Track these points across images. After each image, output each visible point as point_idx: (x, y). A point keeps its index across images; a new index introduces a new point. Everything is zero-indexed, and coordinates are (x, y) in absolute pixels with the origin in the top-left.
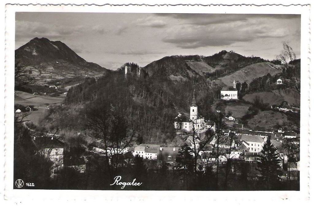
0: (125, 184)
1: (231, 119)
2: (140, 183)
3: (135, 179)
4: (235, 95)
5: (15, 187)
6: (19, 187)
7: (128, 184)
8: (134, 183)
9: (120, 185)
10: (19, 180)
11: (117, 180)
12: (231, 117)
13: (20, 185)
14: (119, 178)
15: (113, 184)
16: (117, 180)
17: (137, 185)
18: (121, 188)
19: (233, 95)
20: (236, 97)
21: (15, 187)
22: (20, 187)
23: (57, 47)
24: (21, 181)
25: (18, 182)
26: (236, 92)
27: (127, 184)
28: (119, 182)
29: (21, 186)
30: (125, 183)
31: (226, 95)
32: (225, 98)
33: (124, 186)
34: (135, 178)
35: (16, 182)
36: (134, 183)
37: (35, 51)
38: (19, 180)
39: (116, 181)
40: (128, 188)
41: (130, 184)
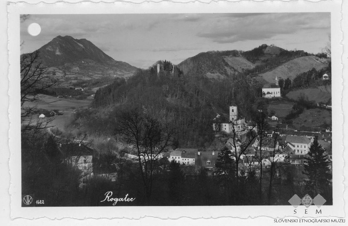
0: (117, 200)
2: (133, 199)
3: (127, 195)
4: (278, 93)
7: (120, 200)
8: (126, 199)
9: (111, 201)
11: (108, 196)
13: (28, 202)
14: (110, 193)
16: (108, 196)
19: (275, 93)
21: (24, 205)
22: (29, 204)
24: (30, 197)
25: (26, 198)
26: (278, 90)
27: (119, 200)
28: (110, 198)
29: (30, 203)
30: (117, 199)
32: (267, 96)
33: (116, 202)
38: (27, 196)
39: (107, 196)
40: (120, 204)
41: (122, 199)
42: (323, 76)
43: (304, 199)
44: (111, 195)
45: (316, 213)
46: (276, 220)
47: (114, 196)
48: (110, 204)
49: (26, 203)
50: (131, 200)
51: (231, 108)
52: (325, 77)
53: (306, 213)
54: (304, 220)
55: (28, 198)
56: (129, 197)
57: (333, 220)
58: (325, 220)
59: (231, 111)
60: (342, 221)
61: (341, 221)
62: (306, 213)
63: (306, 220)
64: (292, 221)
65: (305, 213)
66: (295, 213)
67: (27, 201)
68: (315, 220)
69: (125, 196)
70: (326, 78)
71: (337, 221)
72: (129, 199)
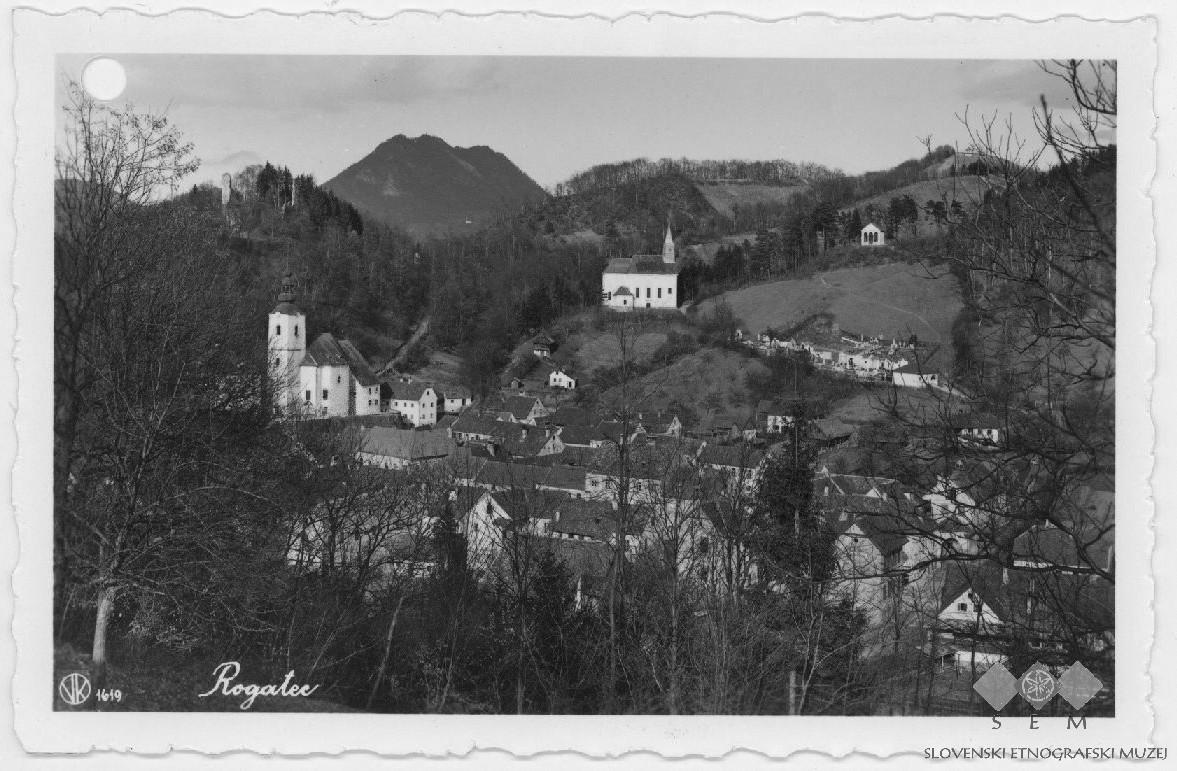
0: (254, 691)
1: (557, 383)
2: (311, 688)
3: (291, 674)
4: (665, 292)
5: (60, 704)
6: (74, 701)
7: (266, 691)
8: (287, 689)
9: (235, 693)
10: (74, 676)
11: (227, 676)
12: (561, 375)
13: (76, 696)
14: (233, 669)
15: (211, 693)
16: (227, 676)
17: (300, 695)
18: (242, 707)
19: (654, 293)
20: (670, 301)
21: (60, 704)
22: (78, 702)
23: (471, 168)
24: (81, 680)
25: (68, 684)
26: (670, 281)
27: (263, 692)
28: (232, 685)
29: (81, 699)
30: (256, 688)
31: (623, 291)
32: (616, 303)
33: (252, 700)
34: (290, 670)
35: (62, 684)
36: (287, 690)
37: (392, 181)
38: (72, 675)
39: (221, 679)
40: (263, 705)
41: (272, 690)
42: (863, 231)
43: (1027, 678)
44: (236, 675)
45: (1069, 728)
46: (930, 752)
47: (245, 678)
48: (231, 705)
49: (69, 700)
50: (302, 691)
51: (276, 319)
52: (872, 237)
53: (1035, 725)
54: (1025, 752)
55: (75, 681)
56: (298, 681)
57: (1127, 752)
58: (1099, 752)
59: (272, 331)
60: (1157, 753)
61: (1154, 754)
62: (1035, 725)
63: (1035, 753)
64: (985, 755)
65: (1032, 727)
66: (997, 725)
67: (70, 691)
68: (1063, 751)
69: (284, 679)
70: (871, 242)
71: (1140, 754)
72: (298, 688)
